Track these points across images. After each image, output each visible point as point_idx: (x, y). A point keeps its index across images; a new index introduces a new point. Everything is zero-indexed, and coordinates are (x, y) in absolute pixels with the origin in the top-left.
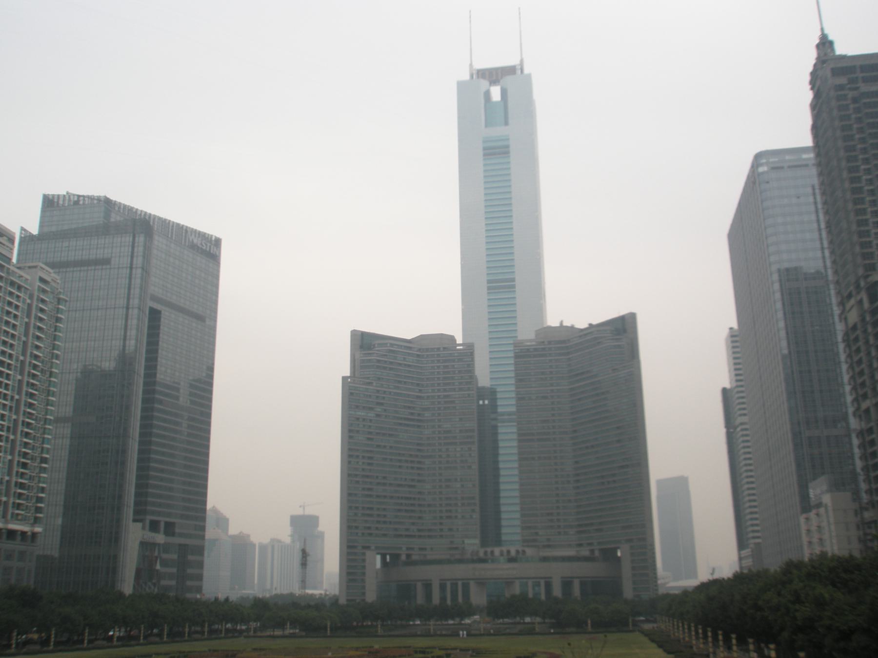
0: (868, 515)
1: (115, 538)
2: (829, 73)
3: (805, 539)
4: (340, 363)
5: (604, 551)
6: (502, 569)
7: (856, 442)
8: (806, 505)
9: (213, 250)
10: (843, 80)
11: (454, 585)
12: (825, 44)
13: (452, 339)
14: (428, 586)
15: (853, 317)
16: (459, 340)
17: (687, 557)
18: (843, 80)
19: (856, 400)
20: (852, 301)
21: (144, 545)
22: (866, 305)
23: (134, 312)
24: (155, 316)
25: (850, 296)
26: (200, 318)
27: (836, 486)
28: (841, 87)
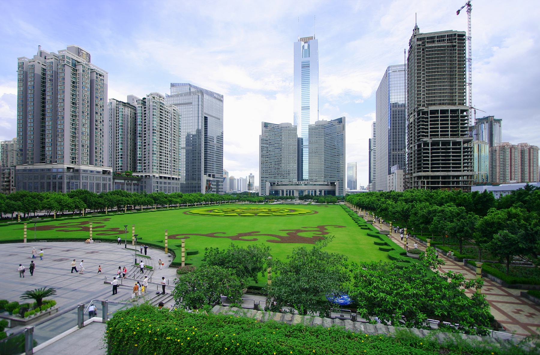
0: (407, 176)
1: (200, 179)
2: (416, 40)
3: (388, 182)
4: (258, 131)
5: (331, 183)
6: (303, 187)
7: (407, 156)
8: (390, 173)
9: (222, 99)
10: (421, 43)
11: (290, 191)
12: (416, 29)
13: (291, 124)
14: (283, 191)
15: (412, 120)
16: (293, 125)
17: (353, 183)
18: (421, 43)
19: (409, 144)
20: (412, 115)
21: (208, 181)
22: (416, 116)
23: (200, 118)
24: (206, 118)
25: (411, 113)
26: (219, 119)
27: (400, 168)
28: (419, 45)
